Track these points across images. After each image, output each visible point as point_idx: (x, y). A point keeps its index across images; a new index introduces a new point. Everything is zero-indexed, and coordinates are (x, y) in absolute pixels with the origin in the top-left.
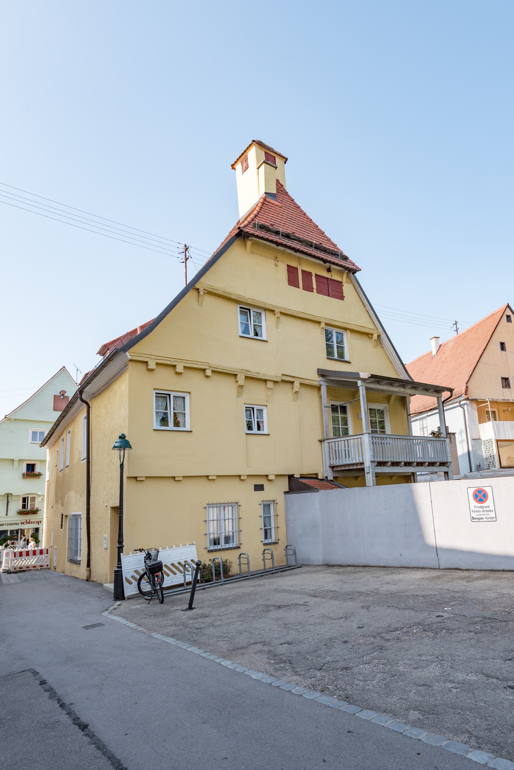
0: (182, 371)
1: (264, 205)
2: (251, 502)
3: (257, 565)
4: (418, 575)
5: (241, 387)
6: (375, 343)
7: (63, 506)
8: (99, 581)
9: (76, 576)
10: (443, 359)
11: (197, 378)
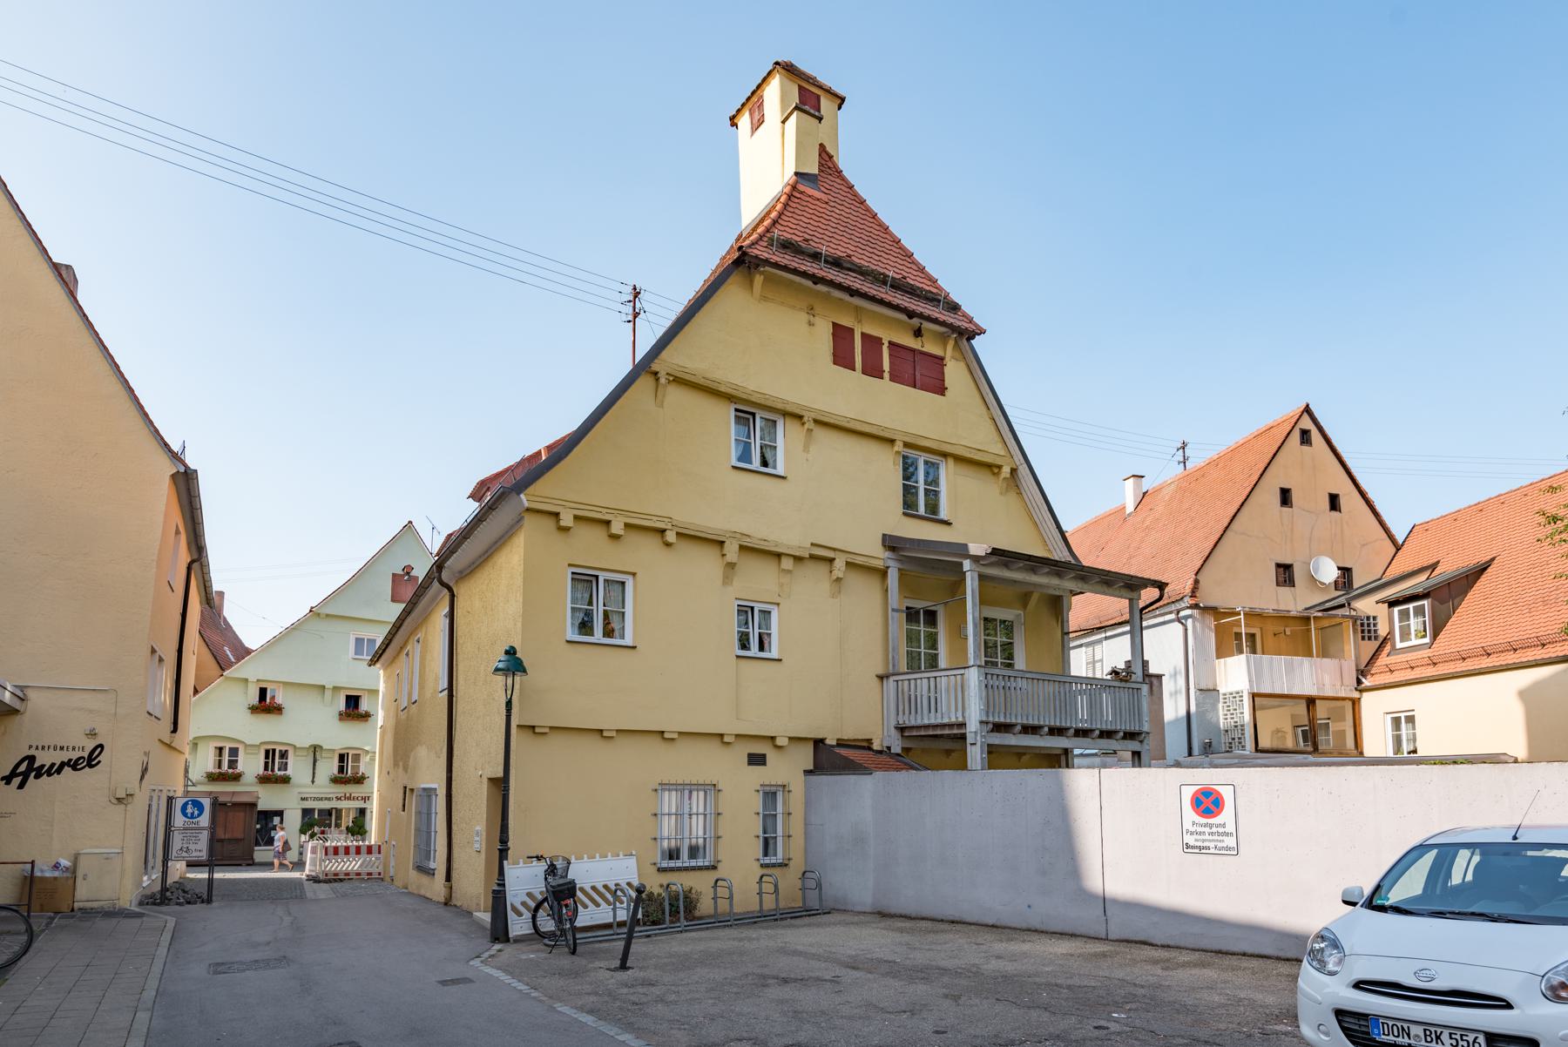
2: (741, 787)
3: (746, 898)
4: (1063, 947)
11: (650, 544)
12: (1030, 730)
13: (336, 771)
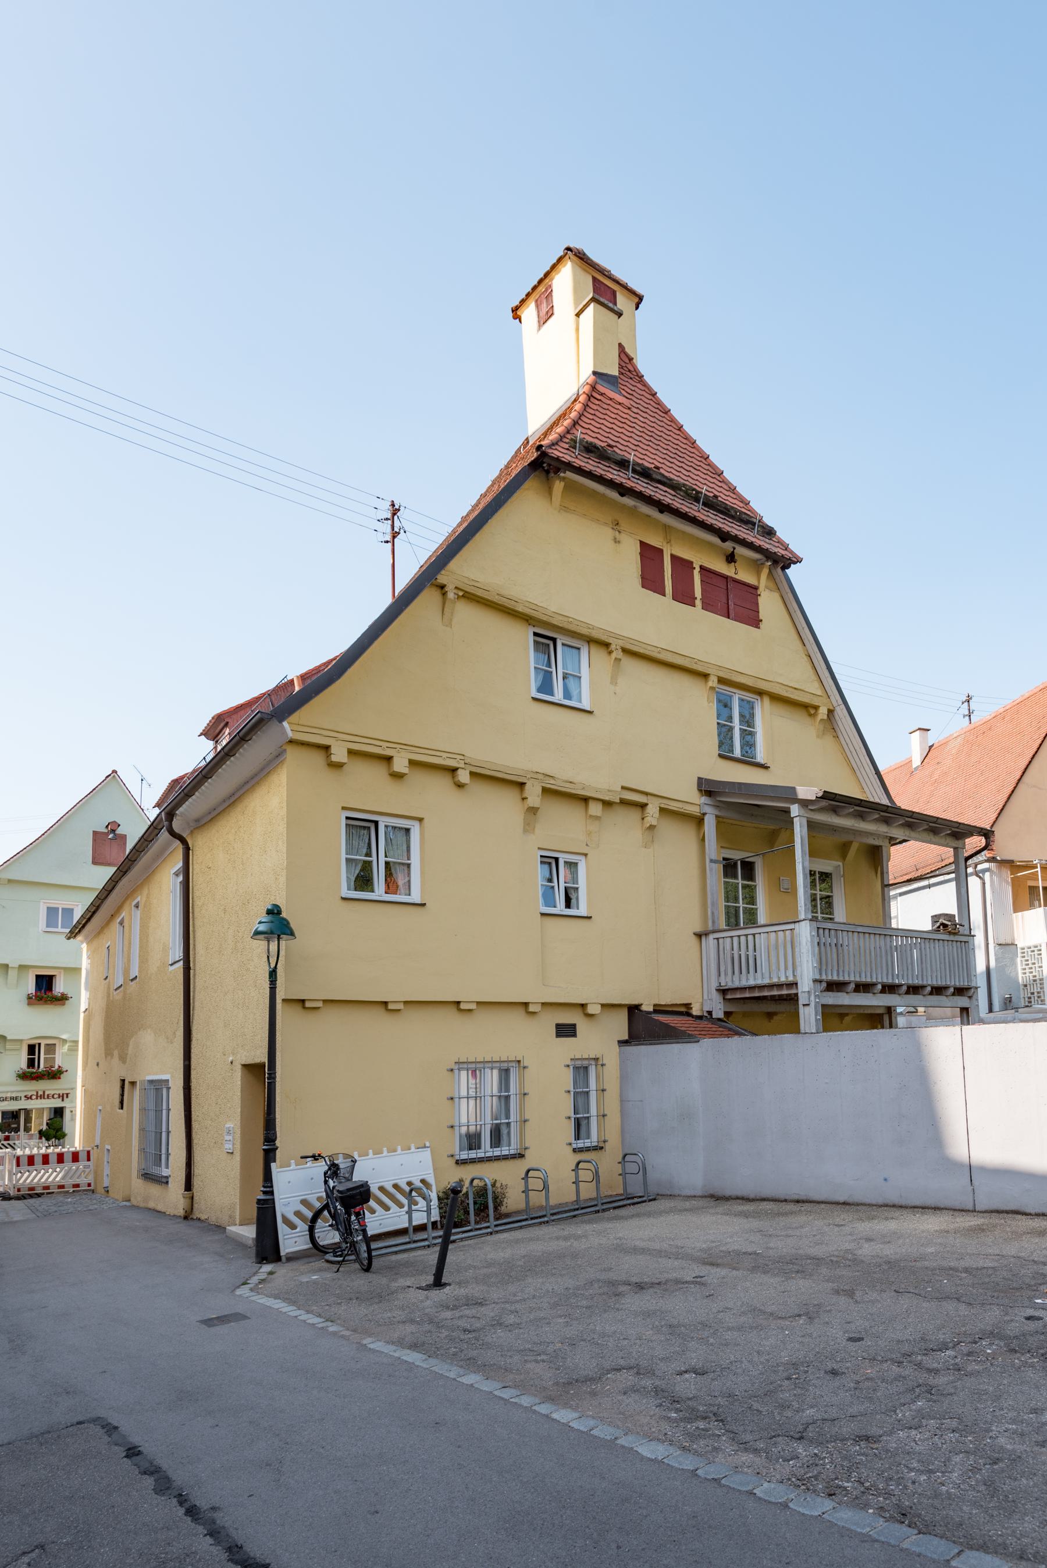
0: (406, 770)
1: (592, 399)
2: (547, 1064)
3: (562, 1192)
4: (931, 1223)
5: (533, 811)
6: (821, 727)
7: (124, 1062)
8: (213, 1220)
9: (159, 1208)
10: (936, 776)
11: (438, 787)
12: (863, 988)
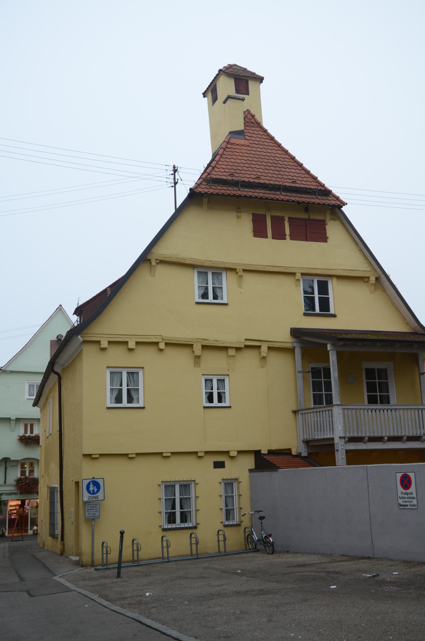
0: (134, 347)
11: (150, 351)
13: (19, 475)
